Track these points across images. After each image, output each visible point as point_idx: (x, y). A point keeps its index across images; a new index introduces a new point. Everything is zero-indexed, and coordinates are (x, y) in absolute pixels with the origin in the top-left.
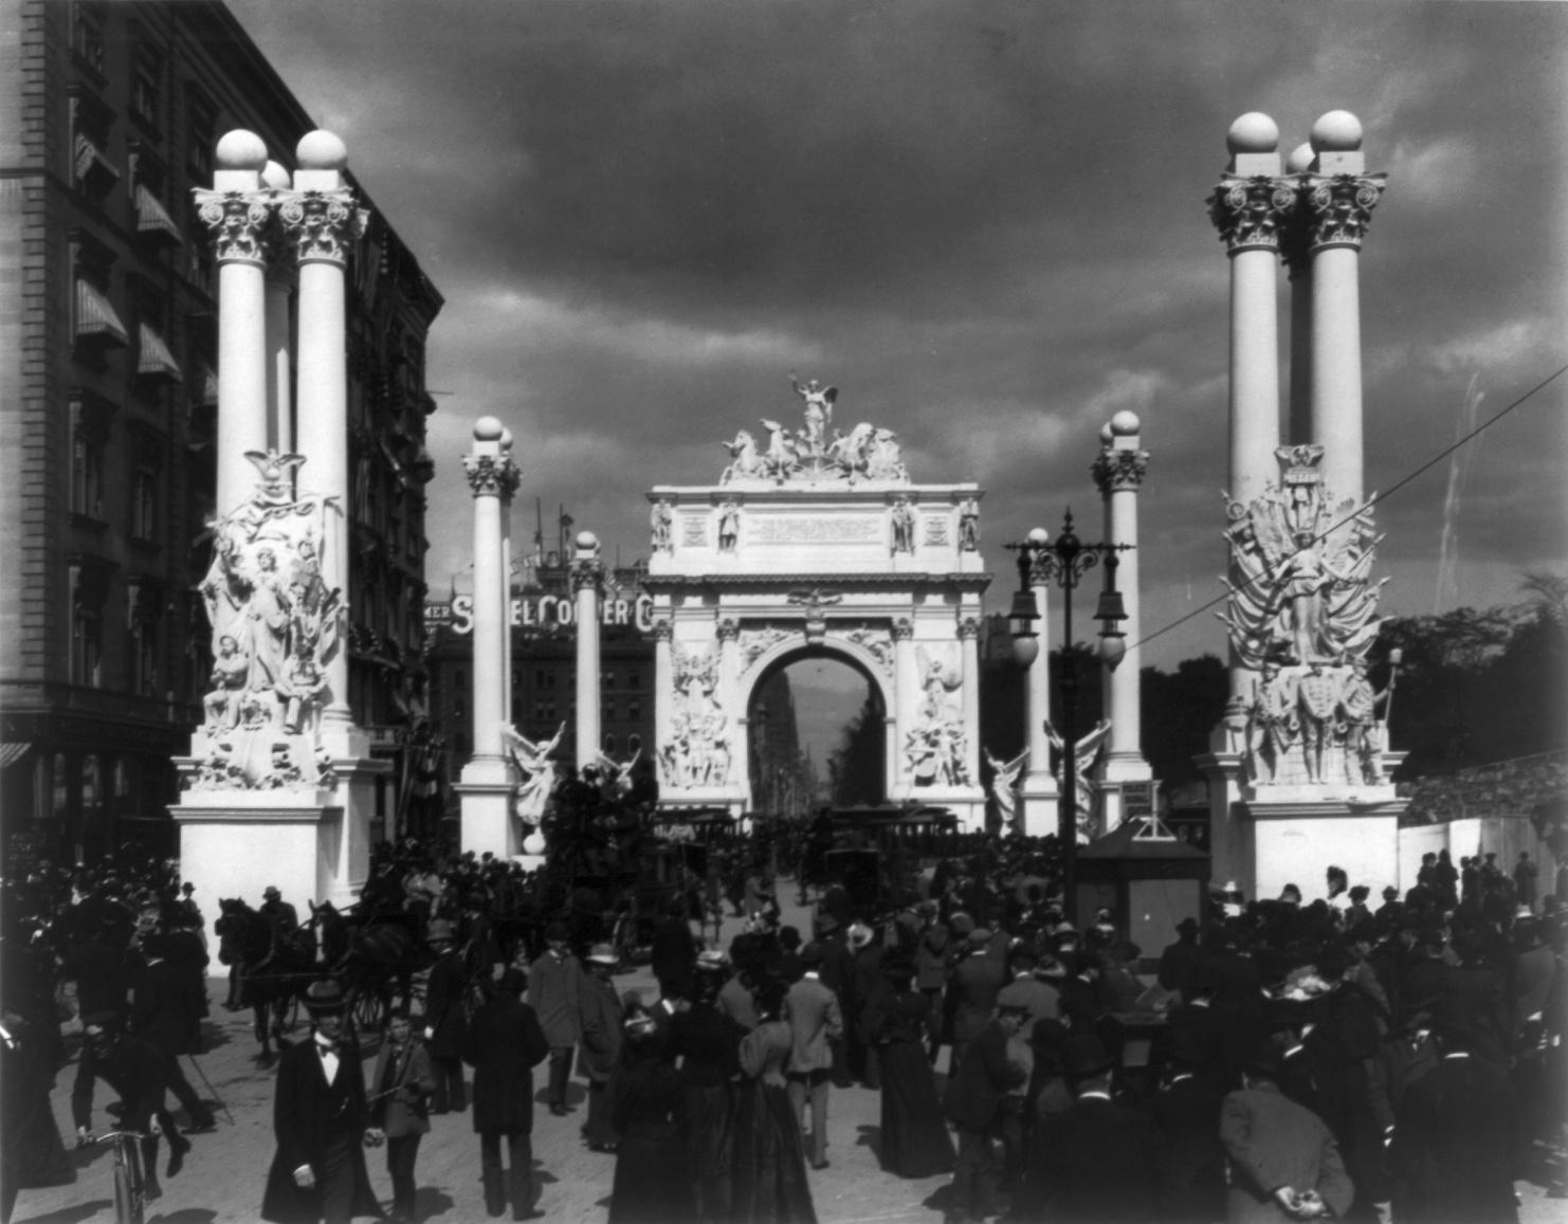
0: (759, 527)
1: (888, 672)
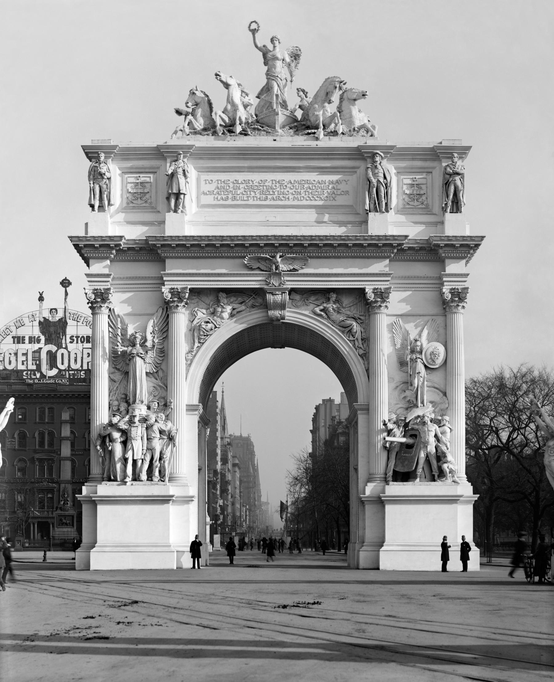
0: (212, 187)
1: (361, 352)
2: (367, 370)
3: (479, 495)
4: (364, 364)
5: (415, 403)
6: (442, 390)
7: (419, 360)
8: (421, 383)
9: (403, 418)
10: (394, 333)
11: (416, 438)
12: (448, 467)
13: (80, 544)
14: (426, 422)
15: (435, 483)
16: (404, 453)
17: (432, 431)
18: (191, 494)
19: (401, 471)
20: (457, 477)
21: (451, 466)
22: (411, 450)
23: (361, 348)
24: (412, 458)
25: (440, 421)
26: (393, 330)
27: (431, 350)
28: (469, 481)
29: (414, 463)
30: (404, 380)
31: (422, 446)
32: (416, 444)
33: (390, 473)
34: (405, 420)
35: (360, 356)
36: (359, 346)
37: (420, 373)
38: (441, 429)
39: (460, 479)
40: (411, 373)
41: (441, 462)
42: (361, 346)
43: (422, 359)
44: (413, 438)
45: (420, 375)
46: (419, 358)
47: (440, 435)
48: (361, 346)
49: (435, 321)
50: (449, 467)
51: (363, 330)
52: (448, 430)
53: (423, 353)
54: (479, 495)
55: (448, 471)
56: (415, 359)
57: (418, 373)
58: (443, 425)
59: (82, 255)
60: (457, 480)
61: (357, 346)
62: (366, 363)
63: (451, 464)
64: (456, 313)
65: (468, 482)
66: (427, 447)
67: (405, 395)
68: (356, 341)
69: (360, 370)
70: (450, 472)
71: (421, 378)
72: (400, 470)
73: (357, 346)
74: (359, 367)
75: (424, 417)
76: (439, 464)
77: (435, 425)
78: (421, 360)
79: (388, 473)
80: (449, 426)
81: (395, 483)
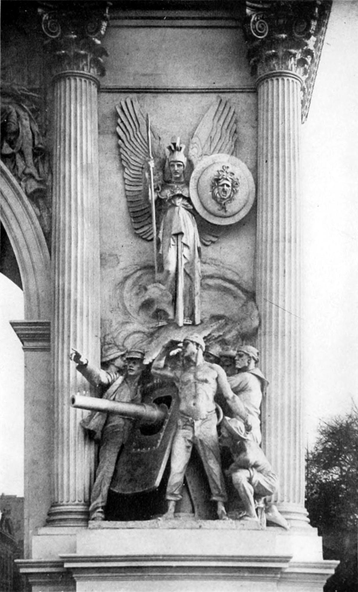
1: (33, 185)
2: (48, 236)
3: (338, 562)
4: (40, 218)
5: (171, 317)
6: (244, 286)
7: (179, 202)
8: (184, 261)
9: (138, 356)
10: (119, 137)
11: (169, 405)
12: (250, 480)
13: (333, 577)
14: (193, 359)
15: (216, 522)
16: (136, 448)
17: (206, 381)
18: (78, 551)
19: (126, 493)
20: (280, 512)
21: (257, 477)
22: (154, 437)
23: (31, 176)
24: (157, 456)
25: (232, 359)
26: (118, 129)
27: (212, 173)
28: (313, 523)
29: (158, 468)
30: (143, 259)
31: (180, 422)
32: (167, 420)
33: (100, 501)
34: (141, 360)
35: (30, 196)
36: (27, 171)
37: (182, 234)
38: (237, 379)
39: (288, 517)
40: (160, 236)
41: (233, 466)
42: (32, 170)
43: (189, 200)
44: (162, 408)
45: (184, 240)
46: (180, 196)
47: (229, 393)
48: (32, 170)
49: (228, 105)
50: (254, 481)
51: (36, 129)
52: (254, 384)
53: (192, 183)
54: (338, 562)
55: (250, 490)
56: (170, 201)
57: (176, 235)
58: (244, 369)
59: (102, 353)
60: (280, 519)
61: (21, 170)
62: (45, 214)
63: (260, 472)
64: (281, 75)
65: (310, 527)
66: (192, 425)
67: (147, 297)
68: (18, 156)
69: (30, 235)
70: (257, 496)
71: (186, 249)
72: (123, 490)
73: (21, 170)
74: (26, 224)
75: (186, 344)
76: (227, 472)
77: (215, 366)
78: (186, 203)
79: (94, 500)
80: (258, 372)
81: (112, 524)
